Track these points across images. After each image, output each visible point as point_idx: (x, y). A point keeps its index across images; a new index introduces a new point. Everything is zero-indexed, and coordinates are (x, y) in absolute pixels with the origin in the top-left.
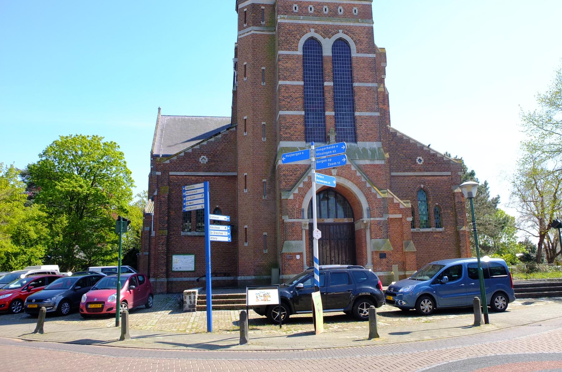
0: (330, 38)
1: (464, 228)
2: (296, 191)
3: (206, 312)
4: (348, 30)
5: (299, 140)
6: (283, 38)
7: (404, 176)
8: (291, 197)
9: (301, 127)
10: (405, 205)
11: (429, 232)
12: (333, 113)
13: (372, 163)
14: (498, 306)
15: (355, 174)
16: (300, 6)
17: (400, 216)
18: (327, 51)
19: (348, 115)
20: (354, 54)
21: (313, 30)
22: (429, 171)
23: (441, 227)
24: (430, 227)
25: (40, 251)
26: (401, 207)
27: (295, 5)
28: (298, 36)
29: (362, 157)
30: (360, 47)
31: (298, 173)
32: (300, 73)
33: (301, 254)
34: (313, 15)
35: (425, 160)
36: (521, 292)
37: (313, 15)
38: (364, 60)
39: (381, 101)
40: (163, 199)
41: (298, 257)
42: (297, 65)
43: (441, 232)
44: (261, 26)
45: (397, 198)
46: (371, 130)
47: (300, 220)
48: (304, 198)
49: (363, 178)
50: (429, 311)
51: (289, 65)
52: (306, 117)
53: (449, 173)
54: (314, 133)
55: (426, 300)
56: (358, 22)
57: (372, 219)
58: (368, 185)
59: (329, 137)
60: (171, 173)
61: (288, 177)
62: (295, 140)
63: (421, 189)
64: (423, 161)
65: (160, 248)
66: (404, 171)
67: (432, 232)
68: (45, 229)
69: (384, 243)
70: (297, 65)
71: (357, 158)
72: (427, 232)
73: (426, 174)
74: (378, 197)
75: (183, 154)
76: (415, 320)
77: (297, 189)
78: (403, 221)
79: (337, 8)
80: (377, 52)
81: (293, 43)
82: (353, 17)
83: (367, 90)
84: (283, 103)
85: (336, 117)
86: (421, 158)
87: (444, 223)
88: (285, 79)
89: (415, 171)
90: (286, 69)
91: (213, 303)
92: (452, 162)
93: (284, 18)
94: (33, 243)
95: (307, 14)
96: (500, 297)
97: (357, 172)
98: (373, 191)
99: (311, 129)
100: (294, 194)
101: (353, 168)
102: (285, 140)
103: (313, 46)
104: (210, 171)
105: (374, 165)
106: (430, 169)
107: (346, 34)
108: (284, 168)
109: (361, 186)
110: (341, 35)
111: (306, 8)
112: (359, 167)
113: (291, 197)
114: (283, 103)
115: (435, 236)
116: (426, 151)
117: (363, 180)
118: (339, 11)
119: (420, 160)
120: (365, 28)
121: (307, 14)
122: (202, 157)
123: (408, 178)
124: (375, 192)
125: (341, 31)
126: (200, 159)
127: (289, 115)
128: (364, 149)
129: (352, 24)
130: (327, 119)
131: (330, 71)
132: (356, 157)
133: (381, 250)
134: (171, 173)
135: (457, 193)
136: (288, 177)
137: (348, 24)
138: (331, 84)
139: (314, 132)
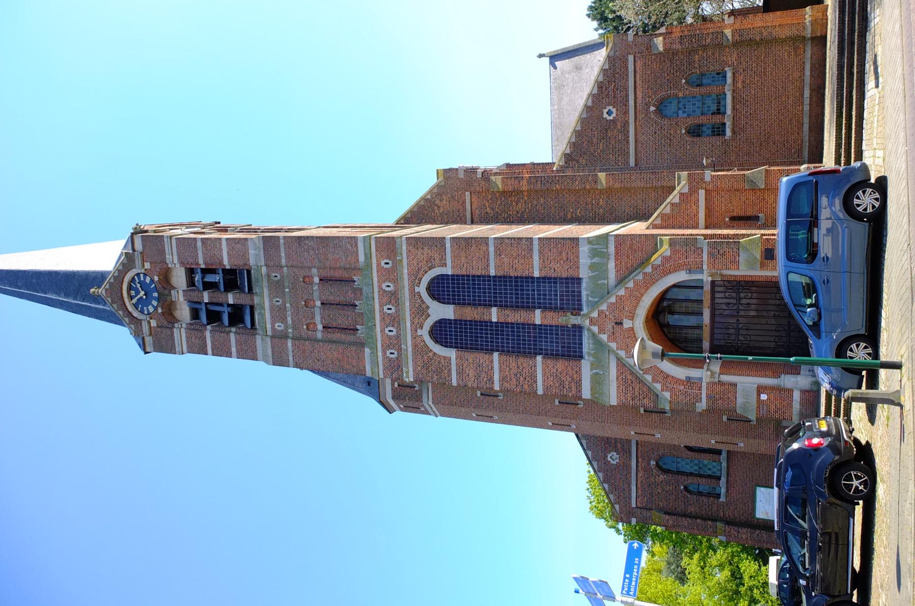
0: (428, 307)
1: (728, 32)
2: (658, 386)
3: (854, 404)
4: (415, 279)
5: (580, 369)
6: (435, 377)
7: (636, 142)
8: (667, 395)
9: (561, 365)
10: (683, 183)
11: (733, 98)
12: (538, 312)
13: (612, 257)
14: (873, 207)
15: (631, 290)
16: (389, 347)
17: (702, 193)
18: (447, 312)
19: (539, 286)
20: (448, 271)
21: (419, 332)
22: (627, 96)
24: (724, 124)
25: (748, 566)
26: (686, 190)
27: (388, 354)
28: (430, 354)
29: (604, 274)
30: (437, 261)
31: (629, 377)
32: (482, 357)
33: (760, 389)
34: (399, 329)
37: (399, 329)
38: (455, 257)
39: (517, 182)
40: (671, 522)
41: (764, 397)
42: (470, 360)
43: (734, 74)
44: (420, 391)
45: (671, 197)
46: (561, 253)
47: (704, 385)
48: (668, 376)
49: (637, 278)
50: (870, 350)
51: (471, 373)
52: (547, 355)
53: (631, 58)
54: (569, 343)
55: (856, 201)
56: (401, 261)
57: (705, 267)
58: (649, 269)
59: (574, 326)
60: (634, 505)
61: (637, 393)
63: (659, 111)
64: (611, 108)
65: (744, 536)
66: (628, 142)
67: (733, 91)
68: (718, 556)
69: (747, 250)
70: (470, 360)
71: (606, 282)
72: (733, 102)
74: (668, 253)
75: (606, 486)
76: (887, 324)
77: (655, 384)
78: (710, 187)
79: (385, 291)
80: (443, 183)
81: (439, 362)
82: (394, 268)
83: (500, 255)
84: (526, 387)
85: (544, 308)
86: (605, 111)
88: (491, 380)
90: (477, 377)
91: (848, 162)
92: (612, 53)
93: (407, 372)
94: (736, 576)
95: (398, 337)
96: (856, 201)
97: (627, 286)
98: (659, 262)
99: (563, 347)
100: (662, 390)
101: (622, 292)
102: (580, 391)
103: (443, 332)
104: (630, 452)
105: (617, 254)
106: (623, 94)
107: (420, 280)
108: (623, 398)
109: (650, 281)
110: (422, 289)
111: (390, 337)
112: (621, 281)
113: (667, 395)
114: (526, 387)
115: (740, 85)
116: (593, 102)
117: (640, 277)
118: (389, 312)
119: (610, 113)
120: (409, 251)
121: (398, 337)
122: (609, 459)
124: (660, 259)
126: (612, 462)
127: (544, 381)
128: (592, 267)
129: (405, 271)
130: (547, 322)
131: (475, 312)
132: (604, 284)
133: (759, 257)
134: (634, 505)
135: (665, 44)
136: (637, 393)
137: (406, 277)
138: (494, 310)
139: (567, 346)
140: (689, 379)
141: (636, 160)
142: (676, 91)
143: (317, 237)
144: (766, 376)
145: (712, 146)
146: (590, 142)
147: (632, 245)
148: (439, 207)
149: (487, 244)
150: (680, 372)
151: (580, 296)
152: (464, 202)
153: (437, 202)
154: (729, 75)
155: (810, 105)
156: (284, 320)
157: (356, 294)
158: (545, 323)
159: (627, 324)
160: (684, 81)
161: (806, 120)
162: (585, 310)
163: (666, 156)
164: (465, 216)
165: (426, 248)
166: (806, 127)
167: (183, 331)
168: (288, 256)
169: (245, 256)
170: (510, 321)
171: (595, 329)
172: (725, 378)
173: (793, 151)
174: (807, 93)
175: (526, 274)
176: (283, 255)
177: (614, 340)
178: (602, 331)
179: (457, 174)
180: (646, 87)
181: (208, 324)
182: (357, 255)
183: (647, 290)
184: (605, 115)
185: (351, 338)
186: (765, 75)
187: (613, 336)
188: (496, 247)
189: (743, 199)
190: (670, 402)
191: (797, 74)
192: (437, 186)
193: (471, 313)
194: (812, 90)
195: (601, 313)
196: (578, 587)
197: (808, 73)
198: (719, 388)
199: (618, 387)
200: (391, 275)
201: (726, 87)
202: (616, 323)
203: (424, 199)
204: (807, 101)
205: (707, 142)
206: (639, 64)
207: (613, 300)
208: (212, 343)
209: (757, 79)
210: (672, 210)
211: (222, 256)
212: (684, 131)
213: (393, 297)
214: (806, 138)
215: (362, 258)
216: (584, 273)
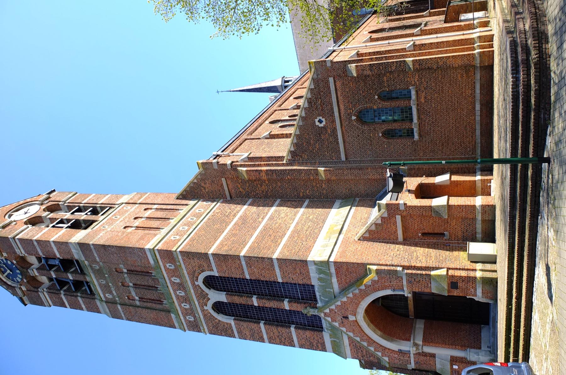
0: (207, 294)
2: (380, 354)
11: (418, 110)
17: (398, 218)
18: (222, 297)
20: (215, 273)
22: (332, 109)
23: (410, 92)
24: (411, 109)
26: (386, 215)
33: (454, 360)
35: (319, 115)
36: (519, 327)
38: (218, 266)
39: (258, 174)
43: (417, 92)
46: (295, 269)
47: (412, 356)
49: (355, 292)
53: (331, 80)
56: (180, 266)
62: (323, 340)
63: (360, 119)
64: (321, 118)
66: (338, 143)
67: (418, 105)
73: (336, 114)
81: (224, 326)
87: (403, 86)
89: (335, 128)
92: (315, 76)
95: (191, 309)
97: (348, 296)
109: (364, 294)
110: (200, 282)
113: (386, 359)
115: (422, 100)
116: (306, 113)
119: (320, 122)
120: (184, 260)
121: (191, 309)
123: (346, 137)
125: (196, 283)
129: (185, 272)
133: (446, 287)
140: (400, 351)
141: (346, 155)
142: (372, 105)
143: (116, 246)
144: (456, 349)
145: (405, 145)
146: (308, 143)
147: (347, 269)
148: (205, 188)
149: (240, 260)
150: (393, 346)
151: (315, 296)
152: (222, 185)
153: (203, 184)
154: (413, 93)
155: (481, 116)
156: (111, 293)
157: (155, 282)
158: (292, 309)
159: (351, 318)
160: (376, 97)
161: (478, 127)
162: (319, 304)
163: (369, 152)
164: (225, 194)
165: (195, 259)
166: (478, 132)
167: (45, 293)
168: (99, 256)
169: (70, 252)
170: (267, 306)
171: (329, 319)
172: (428, 349)
173: (468, 149)
174: (478, 107)
175: (272, 279)
176: (96, 255)
177: (344, 326)
178: (334, 320)
179: (212, 166)
180: (346, 101)
181: (61, 289)
182: (148, 260)
183: (363, 299)
184: (317, 123)
185: (158, 306)
186: (443, 92)
187: (342, 324)
188: (246, 262)
189: (431, 222)
190: (389, 363)
191: (469, 92)
192: (200, 174)
193: (237, 300)
194: (481, 105)
195: (331, 310)
197: (478, 91)
198: (422, 358)
199: (351, 350)
200: (176, 272)
201: (412, 102)
202: (344, 317)
203: (192, 182)
204: (478, 113)
205: (398, 144)
206: (339, 84)
207: (339, 303)
208: (68, 302)
209: (436, 95)
210: (377, 228)
211: (54, 252)
212: (381, 135)
213: (181, 286)
214: (479, 141)
215: (152, 262)
216: (315, 282)
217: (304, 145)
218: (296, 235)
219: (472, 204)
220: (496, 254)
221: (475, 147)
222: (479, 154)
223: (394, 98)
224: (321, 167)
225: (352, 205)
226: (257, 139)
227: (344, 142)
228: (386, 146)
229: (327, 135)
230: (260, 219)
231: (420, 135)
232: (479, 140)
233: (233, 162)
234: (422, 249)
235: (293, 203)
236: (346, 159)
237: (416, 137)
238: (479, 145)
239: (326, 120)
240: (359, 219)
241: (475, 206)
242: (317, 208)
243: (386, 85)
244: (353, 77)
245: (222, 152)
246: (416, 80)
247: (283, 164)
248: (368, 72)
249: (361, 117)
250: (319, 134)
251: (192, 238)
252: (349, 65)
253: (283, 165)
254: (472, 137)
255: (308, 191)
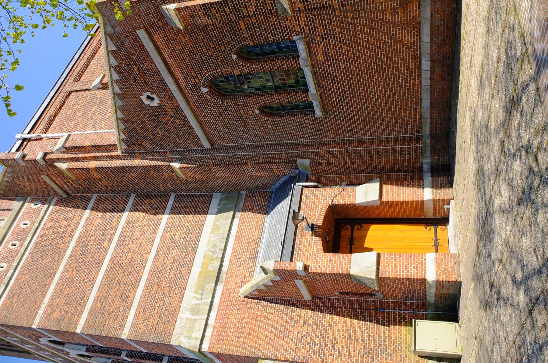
11: (314, 74)
22: (162, 80)
43: (308, 45)
53: (142, 34)
66: (190, 127)
67: (313, 66)
73: (173, 87)
100: (504, 211)
115: (320, 57)
123: (201, 118)
141: (210, 140)
142: (229, 69)
152: (45, 183)
154: (301, 47)
155: (431, 79)
160: (234, 57)
166: (426, 103)
174: (426, 65)
184: (147, 102)
191: (408, 40)
196: (316, 201)
197: (426, 38)
201: (301, 61)
204: (426, 75)
205: (287, 125)
209: (345, 48)
217: (139, 131)
218: (156, 280)
219: (420, 276)
220: (460, 353)
221: (421, 123)
222: (428, 132)
223: (268, 54)
224: (176, 161)
225: (236, 209)
226: (86, 90)
227: (200, 123)
228: (270, 127)
229: (169, 117)
230: (106, 243)
231: (324, 110)
232: (428, 115)
233: (46, 154)
234: (342, 319)
235: (153, 202)
236: (212, 145)
237: (318, 113)
238: (428, 121)
239: (158, 96)
240: (245, 242)
241: (424, 281)
242: (186, 213)
243: (246, 35)
244: (178, 29)
245: (29, 133)
246: (302, 24)
247: (119, 156)
248: (204, 20)
249: (217, 88)
250: (156, 116)
251: (12, 289)
252: (164, 7)
253: (118, 157)
254: (415, 109)
255: (169, 185)
